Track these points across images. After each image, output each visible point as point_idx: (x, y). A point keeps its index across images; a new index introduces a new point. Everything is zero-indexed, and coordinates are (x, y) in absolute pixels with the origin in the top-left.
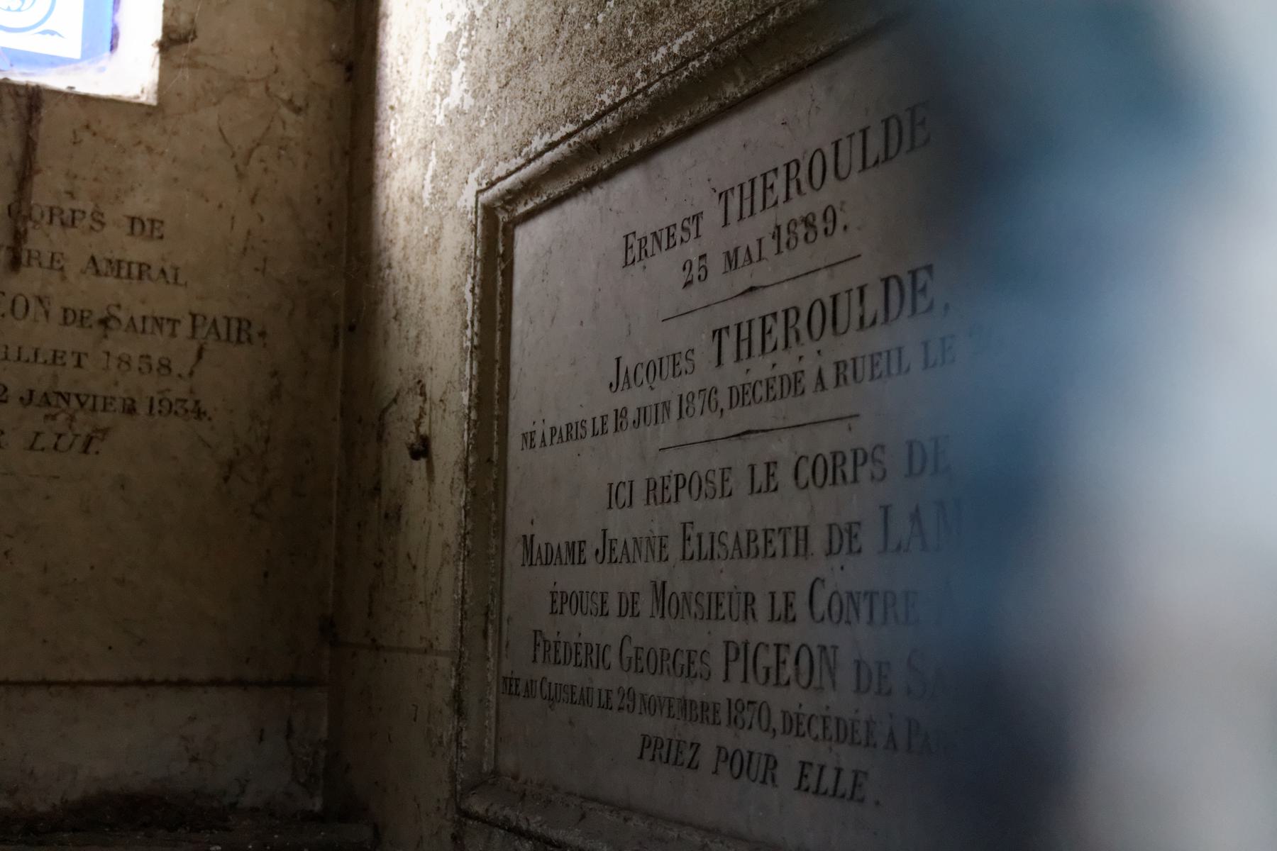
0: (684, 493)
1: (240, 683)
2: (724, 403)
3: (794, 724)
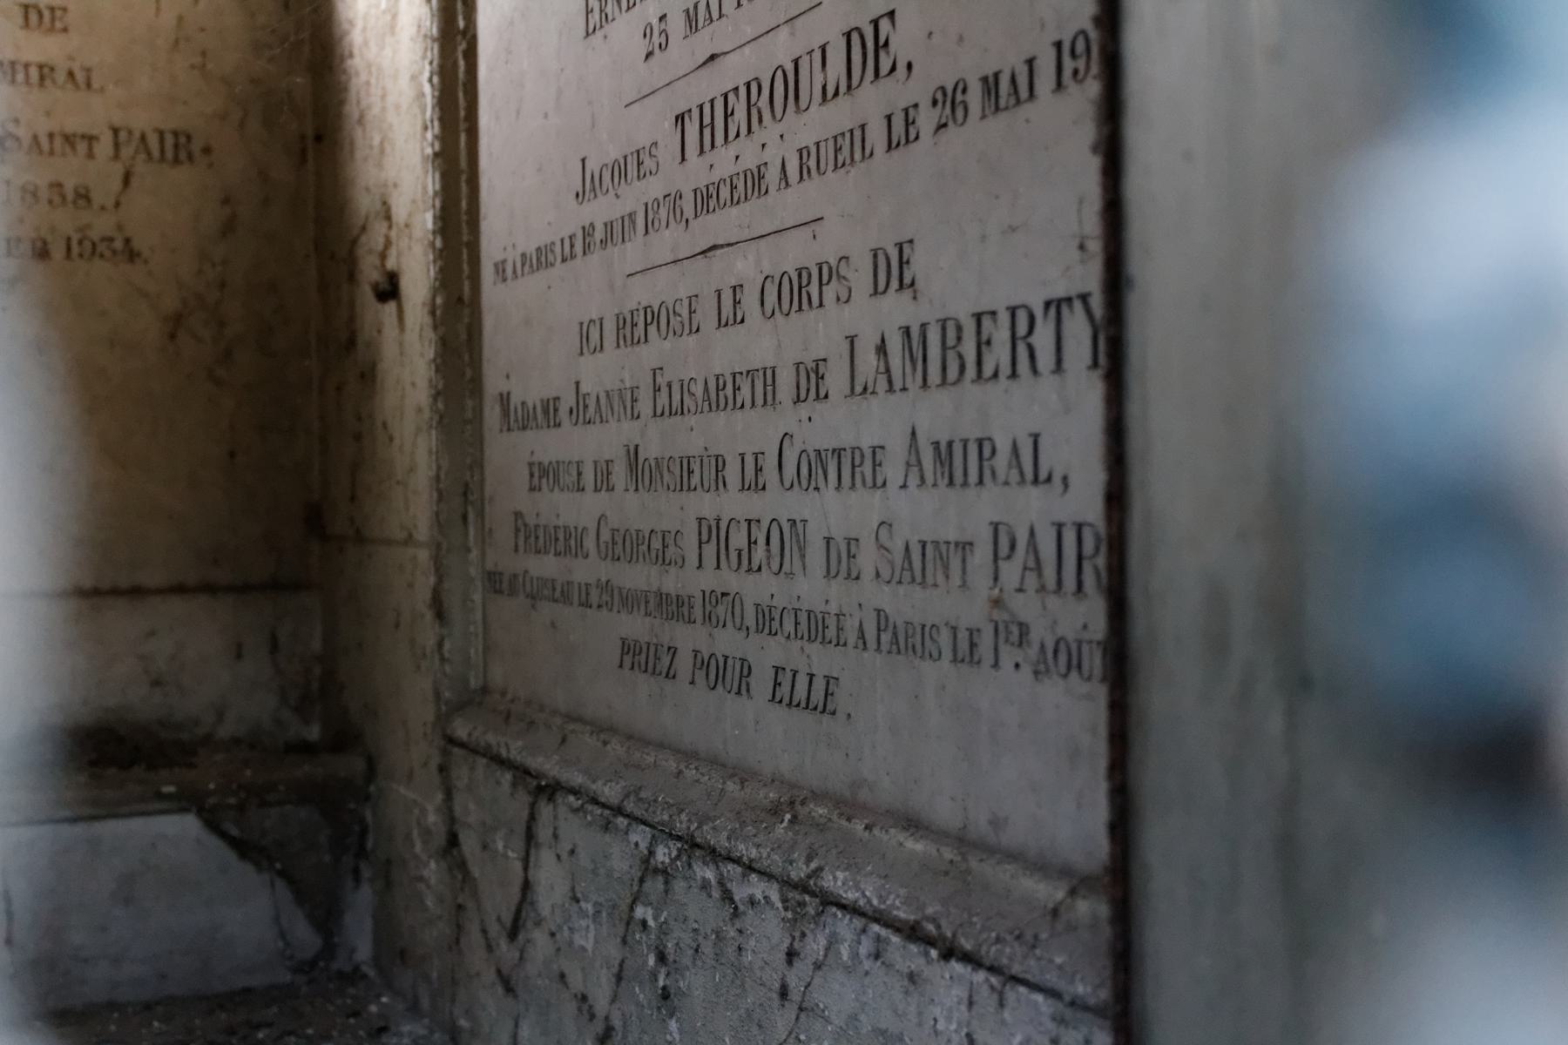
0: (652, 329)
1: (209, 589)
2: (689, 211)
3: (767, 620)
